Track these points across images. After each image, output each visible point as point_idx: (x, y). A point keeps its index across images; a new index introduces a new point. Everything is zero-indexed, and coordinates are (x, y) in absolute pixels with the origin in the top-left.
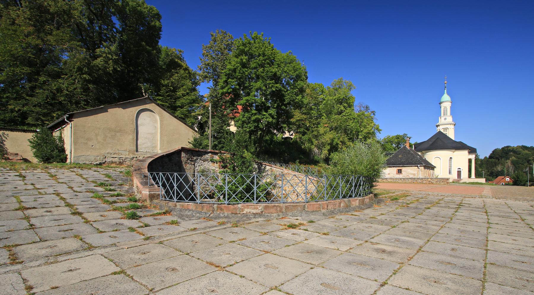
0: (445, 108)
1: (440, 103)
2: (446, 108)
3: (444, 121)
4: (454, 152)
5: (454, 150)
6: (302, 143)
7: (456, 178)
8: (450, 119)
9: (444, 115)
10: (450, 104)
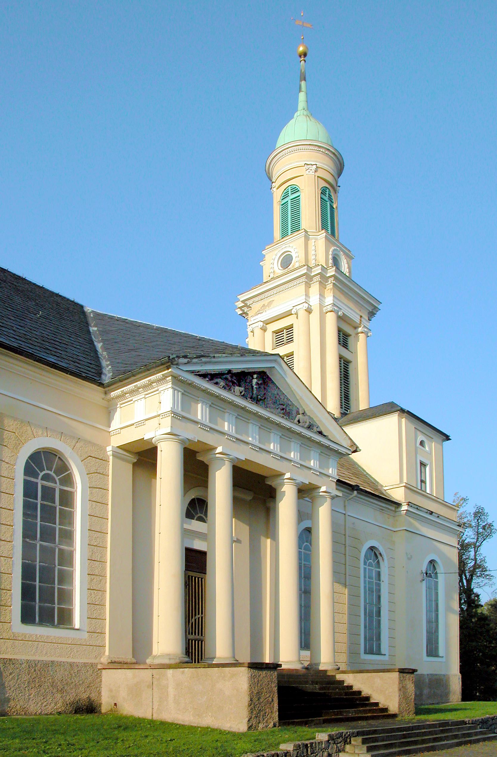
2: (295, 190)
9: (284, 234)
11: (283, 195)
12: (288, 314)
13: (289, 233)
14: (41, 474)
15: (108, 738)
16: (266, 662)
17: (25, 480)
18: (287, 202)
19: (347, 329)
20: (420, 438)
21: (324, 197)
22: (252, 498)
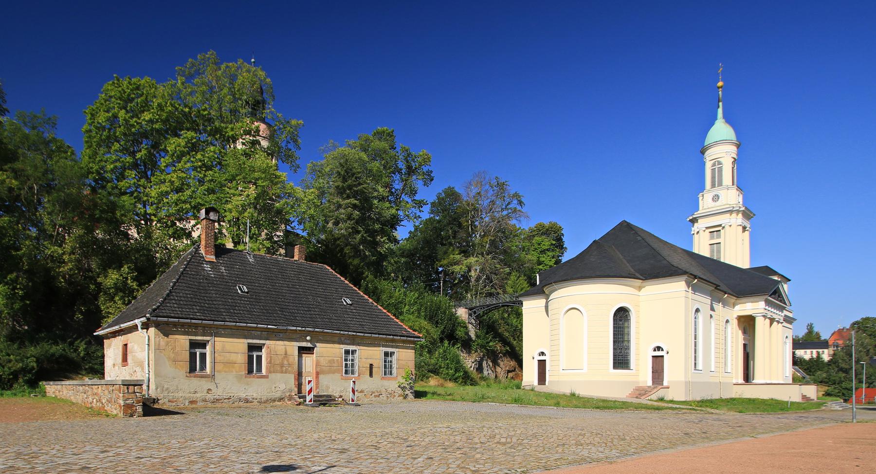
0: (718, 163)
1: (703, 152)
2: (720, 163)
3: (714, 204)
4: (640, 288)
5: (638, 282)
6: (499, 262)
7: (650, 383)
8: (732, 197)
9: (713, 186)
10: (734, 149)
12: (720, 225)
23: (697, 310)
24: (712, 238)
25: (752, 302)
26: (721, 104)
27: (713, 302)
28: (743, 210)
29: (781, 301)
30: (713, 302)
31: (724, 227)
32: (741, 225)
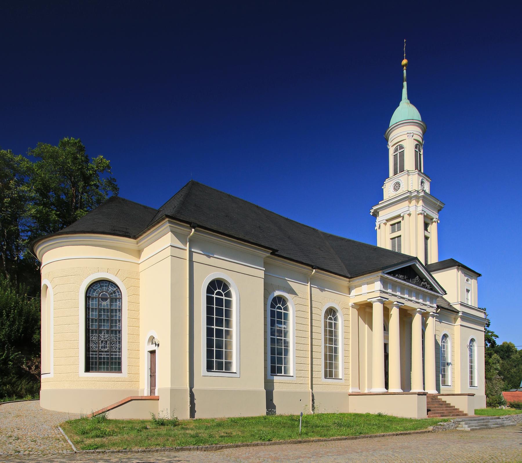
2: (401, 147)
9: (395, 173)
11: (395, 150)
12: (399, 216)
13: (398, 172)
14: (215, 292)
15: (151, 452)
16: (145, 395)
17: (207, 296)
18: (397, 154)
19: (428, 221)
20: (466, 278)
21: (416, 150)
22: (359, 308)
23: (472, 340)
24: (393, 231)
25: (368, 284)
26: (405, 84)
27: (312, 285)
28: (423, 196)
29: (424, 286)
30: (193, 250)
31: (403, 217)
32: (421, 214)
